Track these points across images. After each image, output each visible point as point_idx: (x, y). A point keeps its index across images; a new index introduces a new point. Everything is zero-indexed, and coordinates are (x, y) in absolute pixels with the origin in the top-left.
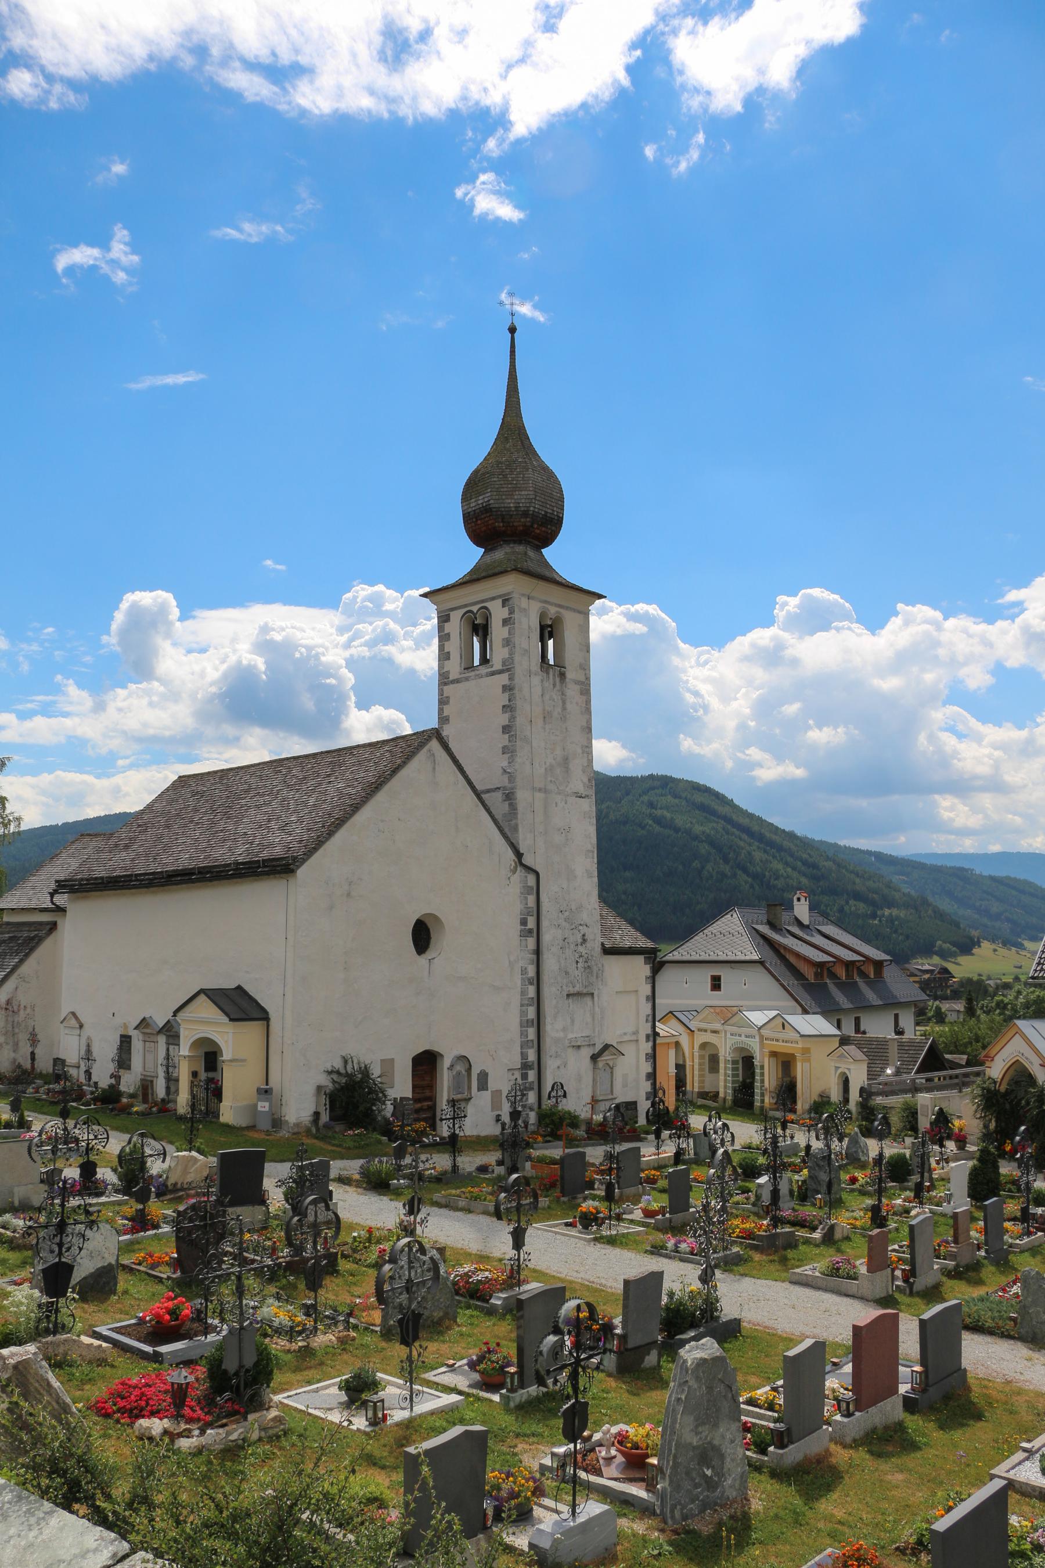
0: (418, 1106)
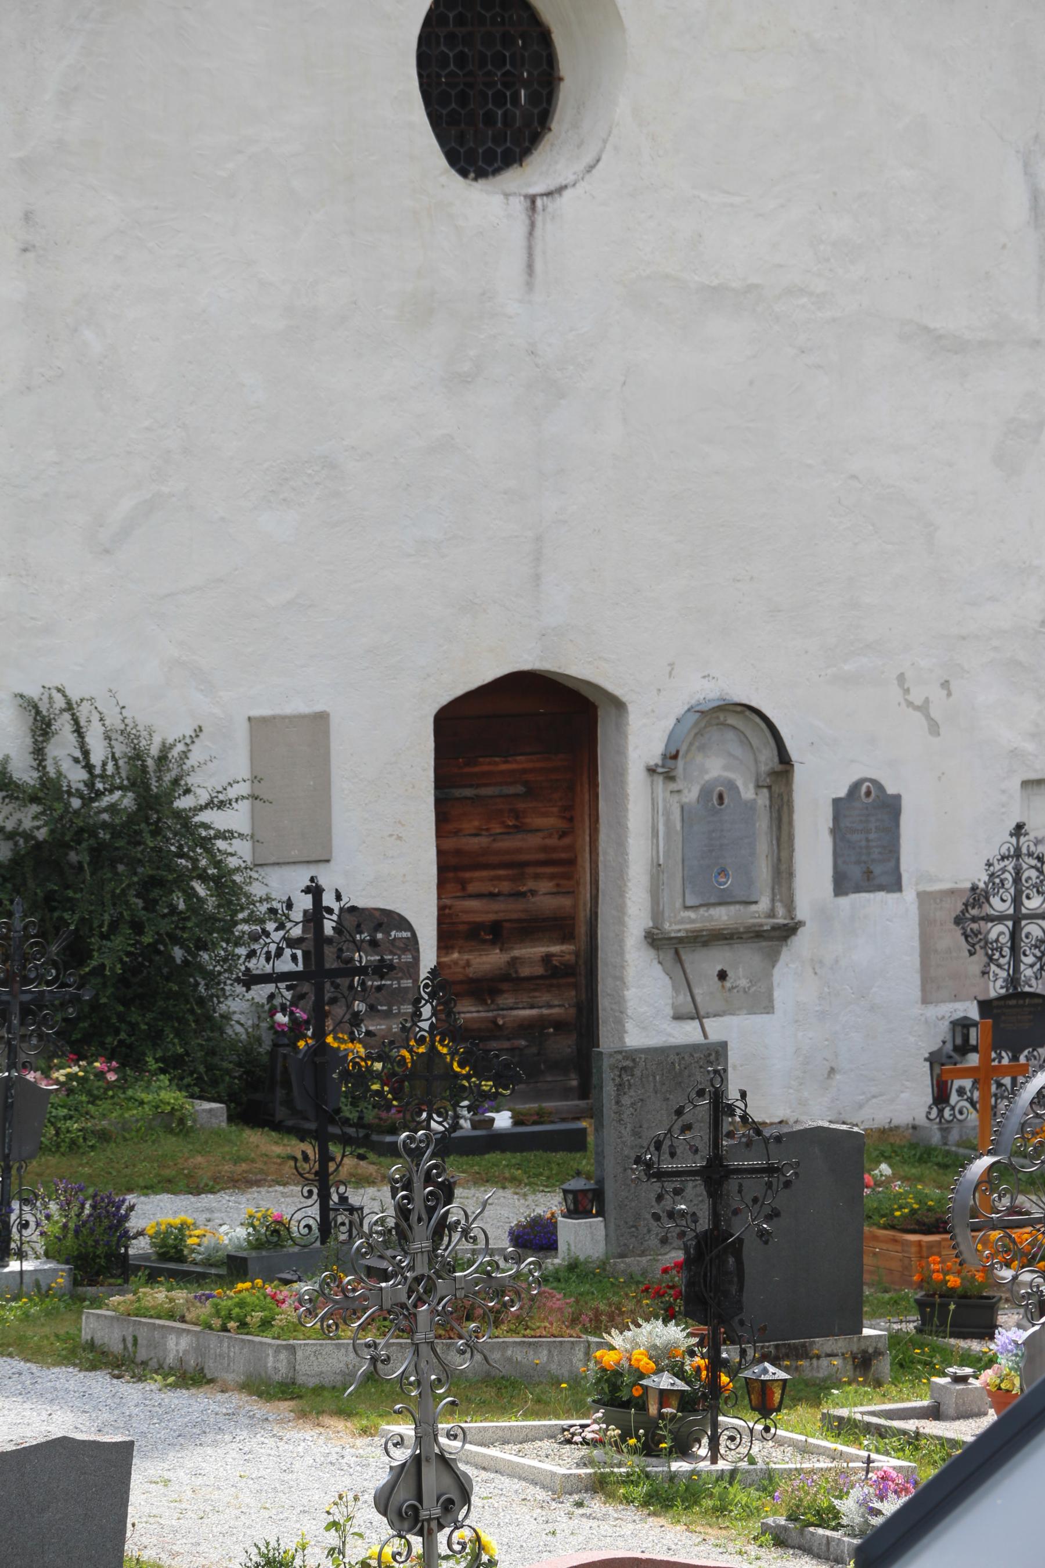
0: (489, 960)
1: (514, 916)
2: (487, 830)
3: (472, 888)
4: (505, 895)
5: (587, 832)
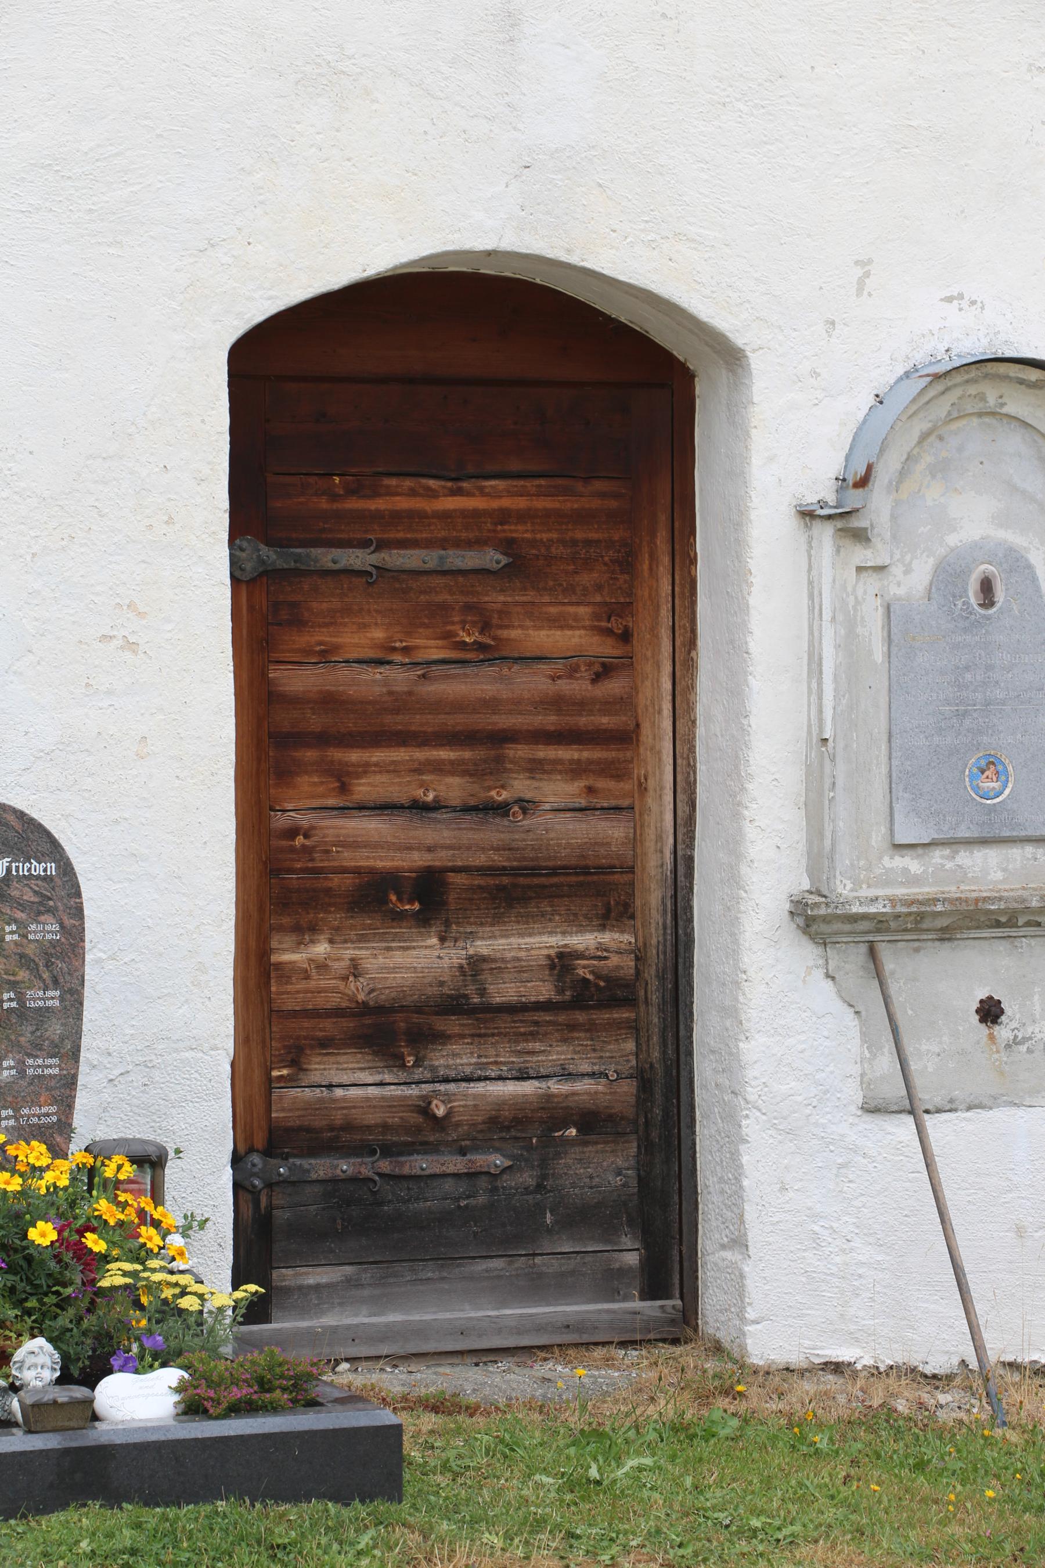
1: (480, 859)
2: (406, 650)
3: (364, 789)
4: (454, 809)
5: (667, 668)
